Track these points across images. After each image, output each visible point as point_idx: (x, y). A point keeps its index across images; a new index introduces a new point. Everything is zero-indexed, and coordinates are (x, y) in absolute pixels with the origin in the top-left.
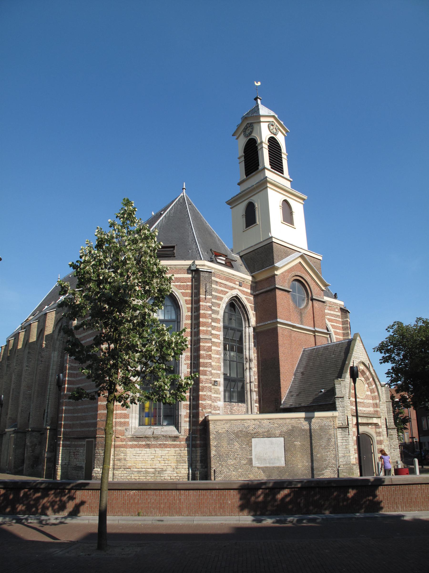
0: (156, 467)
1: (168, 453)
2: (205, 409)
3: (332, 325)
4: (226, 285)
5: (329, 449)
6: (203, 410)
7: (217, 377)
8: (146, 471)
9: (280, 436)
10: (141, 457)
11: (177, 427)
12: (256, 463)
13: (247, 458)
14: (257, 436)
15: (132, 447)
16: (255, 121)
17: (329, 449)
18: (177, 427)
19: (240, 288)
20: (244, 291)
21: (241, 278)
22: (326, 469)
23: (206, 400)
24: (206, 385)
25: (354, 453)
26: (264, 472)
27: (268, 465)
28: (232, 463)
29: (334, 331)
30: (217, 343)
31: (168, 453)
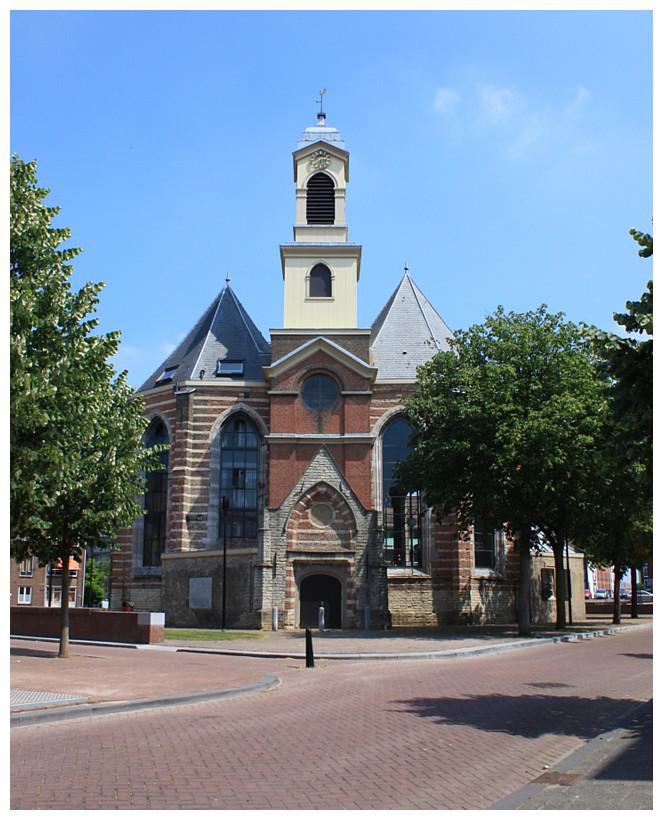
12: (192, 605)
19: (249, 400)
20: (253, 402)
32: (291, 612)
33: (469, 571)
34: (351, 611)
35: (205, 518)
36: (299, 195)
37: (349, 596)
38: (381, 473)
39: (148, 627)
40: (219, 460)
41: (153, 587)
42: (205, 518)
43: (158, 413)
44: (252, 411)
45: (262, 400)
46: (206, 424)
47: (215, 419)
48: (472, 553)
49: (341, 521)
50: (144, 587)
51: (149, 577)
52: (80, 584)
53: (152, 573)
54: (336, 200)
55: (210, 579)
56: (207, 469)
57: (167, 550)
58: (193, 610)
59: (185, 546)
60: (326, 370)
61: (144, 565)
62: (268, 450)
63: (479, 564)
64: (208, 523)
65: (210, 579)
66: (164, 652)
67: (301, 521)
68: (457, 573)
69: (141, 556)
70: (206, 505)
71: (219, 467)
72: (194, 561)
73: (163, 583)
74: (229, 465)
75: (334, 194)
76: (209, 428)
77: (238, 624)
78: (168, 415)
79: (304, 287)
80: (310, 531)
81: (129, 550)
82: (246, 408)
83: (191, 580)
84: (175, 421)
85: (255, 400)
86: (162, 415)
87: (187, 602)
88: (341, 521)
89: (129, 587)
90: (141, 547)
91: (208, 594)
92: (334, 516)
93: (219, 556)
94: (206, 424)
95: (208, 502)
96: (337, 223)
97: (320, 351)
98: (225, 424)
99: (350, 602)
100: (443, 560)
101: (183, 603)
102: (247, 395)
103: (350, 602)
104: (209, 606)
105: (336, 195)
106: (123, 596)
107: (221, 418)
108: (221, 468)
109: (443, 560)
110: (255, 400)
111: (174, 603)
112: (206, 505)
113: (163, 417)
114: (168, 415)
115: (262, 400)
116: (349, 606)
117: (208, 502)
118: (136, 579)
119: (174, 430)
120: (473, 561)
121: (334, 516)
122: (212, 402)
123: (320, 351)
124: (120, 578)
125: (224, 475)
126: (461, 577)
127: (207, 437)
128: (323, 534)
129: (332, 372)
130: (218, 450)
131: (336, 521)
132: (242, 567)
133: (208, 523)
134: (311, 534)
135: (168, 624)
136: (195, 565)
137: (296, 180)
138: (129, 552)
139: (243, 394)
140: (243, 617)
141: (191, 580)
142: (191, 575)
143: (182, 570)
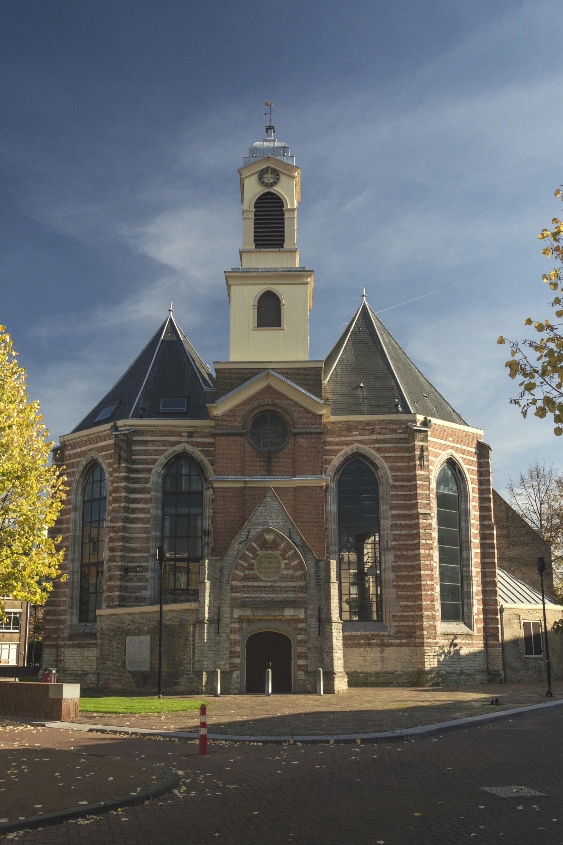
0: (84, 669)
1: (92, 654)
2: (112, 602)
3: (385, 458)
4: (163, 441)
5: (186, 650)
6: (110, 603)
7: (143, 561)
8: (76, 673)
9: (147, 633)
10: (73, 658)
11: (470, 626)
12: (128, 668)
13: (121, 660)
14: (130, 633)
15: (69, 646)
16: (285, 172)
17: (186, 650)
18: (470, 626)
19: (193, 440)
20: (197, 442)
21: (190, 427)
22: (182, 676)
23: (114, 591)
24: (115, 573)
25: (228, 658)
26: (133, 677)
27: (137, 669)
28: (110, 665)
29: (389, 466)
30: (143, 518)
31: (92, 654)
32: (235, 674)
33: (435, 626)
34: (302, 673)
35: (146, 570)
36: (245, 216)
37: (301, 656)
38: (336, 517)
39: (59, 701)
40: (160, 506)
41: (88, 646)
42: (146, 570)
43: (94, 455)
44: (197, 453)
45: (207, 440)
46: (147, 466)
47: (154, 461)
48: (438, 606)
49: (290, 572)
50: (79, 646)
51: (84, 635)
52: (23, 640)
53: (88, 630)
54: (285, 220)
55: (148, 637)
56: (148, 516)
57: (104, 605)
58: (129, 672)
59: (475, 524)
60: (275, 406)
61: (80, 621)
62: (214, 494)
63: (446, 617)
64: (149, 575)
65: (148, 637)
66: (221, 678)
67: (247, 572)
68: (421, 628)
69: (76, 611)
70: (146, 555)
71: (160, 513)
72: (130, 617)
73: (99, 642)
74: (172, 510)
75: (283, 215)
76: (149, 471)
77: (179, 688)
78: (106, 457)
79: (251, 315)
80: (256, 584)
81: (64, 606)
82: (190, 448)
83: (127, 637)
84: (113, 463)
85: (199, 440)
86: (99, 457)
87: (124, 662)
88: (290, 572)
89: (64, 646)
90: (76, 603)
91: (146, 654)
92: (283, 566)
93: (156, 612)
94: (147, 466)
95: (148, 552)
96: (286, 246)
97: (269, 387)
98: (168, 465)
99: (301, 662)
100: (405, 614)
101: (119, 664)
102: (191, 435)
103: (301, 662)
104: (146, 668)
105: (286, 216)
106: (57, 656)
107: (162, 459)
108: (164, 515)
109: (405, 614)
110: (199, 440)
111: (110, 664)
112: (146, 555)
113: (100, 460)
114: (106, 457)
115: (207, 440)
116: (300, 668)
117: (148, 552)
118: (70, 637)
119: (111, 474)
120: (438, 614)
121: (283, 566)
122: (153, 443)
123: (269, 387)
124: (54, 636)
125: (167, 523)
126: (425, 633)
127: (147, 480)
128: (271, 586)
129: (282, 408)
130: (160, 495)
131: (285, 572)
132: (183, 625)
133: (149, 575)
134: (258, 587)
135: (84, 693)
136: (132, 622)
137: (242, 203)
138: (65, 608)
139: (186, 434)
140: (183, 680)
141: (128, 638)
142: (128, 633)
143: (118, 628)
